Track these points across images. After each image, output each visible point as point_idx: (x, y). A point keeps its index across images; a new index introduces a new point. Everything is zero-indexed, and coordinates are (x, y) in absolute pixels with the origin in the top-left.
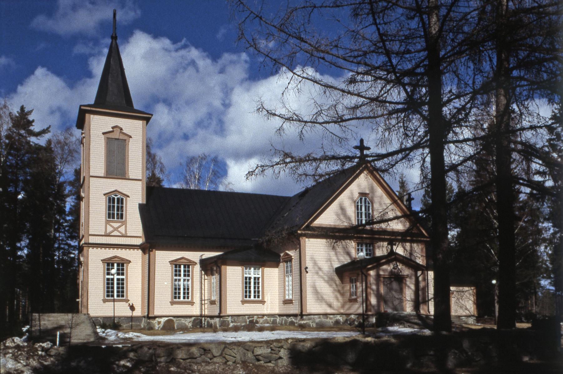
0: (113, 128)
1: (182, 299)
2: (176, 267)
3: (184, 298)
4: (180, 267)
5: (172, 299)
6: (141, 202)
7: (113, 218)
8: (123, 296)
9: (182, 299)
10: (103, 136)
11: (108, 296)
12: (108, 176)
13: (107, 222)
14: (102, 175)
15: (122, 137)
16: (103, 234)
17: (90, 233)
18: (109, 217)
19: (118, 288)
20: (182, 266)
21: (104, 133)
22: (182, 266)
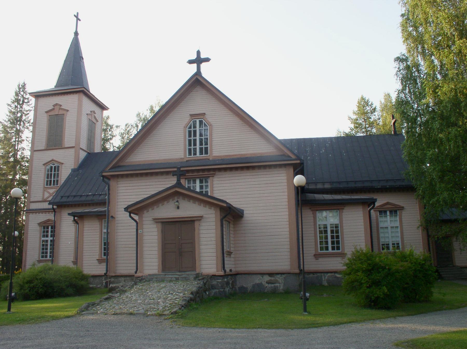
0: (54, 106)
1: (330, 250)
2: (44, 228)
3: (333, 248)
4: (48, 228)
5: (39, 257)
6: (73, 167)
7: (50, 184)
8: (338, 248)
9: (330, 250)
10: (46, 115)
11: (43, 257)
12: (48, 148)
13: (45, 189)
14: (43, 148)
15: (61, 112)
16: (41, 200)
17: (31, 200)
18: (47, 184)
19: (332, 237)
20: (50, 227)
21: (47, 112)
22: (50, 227)
